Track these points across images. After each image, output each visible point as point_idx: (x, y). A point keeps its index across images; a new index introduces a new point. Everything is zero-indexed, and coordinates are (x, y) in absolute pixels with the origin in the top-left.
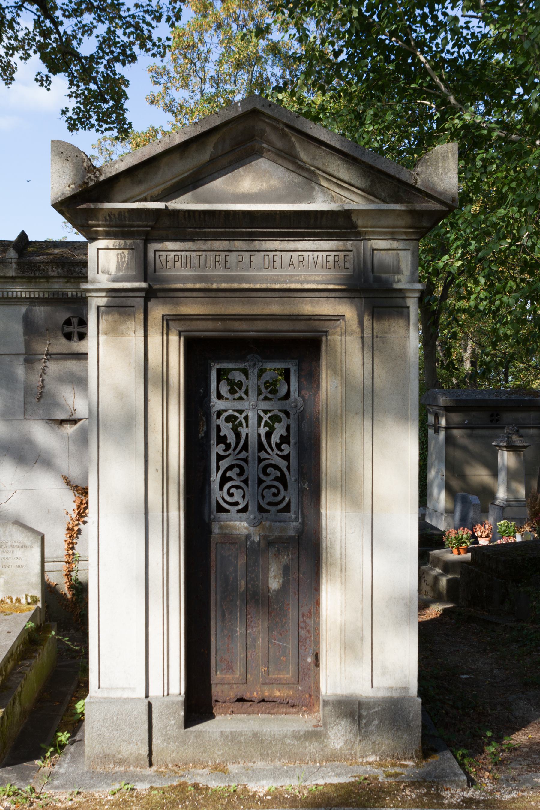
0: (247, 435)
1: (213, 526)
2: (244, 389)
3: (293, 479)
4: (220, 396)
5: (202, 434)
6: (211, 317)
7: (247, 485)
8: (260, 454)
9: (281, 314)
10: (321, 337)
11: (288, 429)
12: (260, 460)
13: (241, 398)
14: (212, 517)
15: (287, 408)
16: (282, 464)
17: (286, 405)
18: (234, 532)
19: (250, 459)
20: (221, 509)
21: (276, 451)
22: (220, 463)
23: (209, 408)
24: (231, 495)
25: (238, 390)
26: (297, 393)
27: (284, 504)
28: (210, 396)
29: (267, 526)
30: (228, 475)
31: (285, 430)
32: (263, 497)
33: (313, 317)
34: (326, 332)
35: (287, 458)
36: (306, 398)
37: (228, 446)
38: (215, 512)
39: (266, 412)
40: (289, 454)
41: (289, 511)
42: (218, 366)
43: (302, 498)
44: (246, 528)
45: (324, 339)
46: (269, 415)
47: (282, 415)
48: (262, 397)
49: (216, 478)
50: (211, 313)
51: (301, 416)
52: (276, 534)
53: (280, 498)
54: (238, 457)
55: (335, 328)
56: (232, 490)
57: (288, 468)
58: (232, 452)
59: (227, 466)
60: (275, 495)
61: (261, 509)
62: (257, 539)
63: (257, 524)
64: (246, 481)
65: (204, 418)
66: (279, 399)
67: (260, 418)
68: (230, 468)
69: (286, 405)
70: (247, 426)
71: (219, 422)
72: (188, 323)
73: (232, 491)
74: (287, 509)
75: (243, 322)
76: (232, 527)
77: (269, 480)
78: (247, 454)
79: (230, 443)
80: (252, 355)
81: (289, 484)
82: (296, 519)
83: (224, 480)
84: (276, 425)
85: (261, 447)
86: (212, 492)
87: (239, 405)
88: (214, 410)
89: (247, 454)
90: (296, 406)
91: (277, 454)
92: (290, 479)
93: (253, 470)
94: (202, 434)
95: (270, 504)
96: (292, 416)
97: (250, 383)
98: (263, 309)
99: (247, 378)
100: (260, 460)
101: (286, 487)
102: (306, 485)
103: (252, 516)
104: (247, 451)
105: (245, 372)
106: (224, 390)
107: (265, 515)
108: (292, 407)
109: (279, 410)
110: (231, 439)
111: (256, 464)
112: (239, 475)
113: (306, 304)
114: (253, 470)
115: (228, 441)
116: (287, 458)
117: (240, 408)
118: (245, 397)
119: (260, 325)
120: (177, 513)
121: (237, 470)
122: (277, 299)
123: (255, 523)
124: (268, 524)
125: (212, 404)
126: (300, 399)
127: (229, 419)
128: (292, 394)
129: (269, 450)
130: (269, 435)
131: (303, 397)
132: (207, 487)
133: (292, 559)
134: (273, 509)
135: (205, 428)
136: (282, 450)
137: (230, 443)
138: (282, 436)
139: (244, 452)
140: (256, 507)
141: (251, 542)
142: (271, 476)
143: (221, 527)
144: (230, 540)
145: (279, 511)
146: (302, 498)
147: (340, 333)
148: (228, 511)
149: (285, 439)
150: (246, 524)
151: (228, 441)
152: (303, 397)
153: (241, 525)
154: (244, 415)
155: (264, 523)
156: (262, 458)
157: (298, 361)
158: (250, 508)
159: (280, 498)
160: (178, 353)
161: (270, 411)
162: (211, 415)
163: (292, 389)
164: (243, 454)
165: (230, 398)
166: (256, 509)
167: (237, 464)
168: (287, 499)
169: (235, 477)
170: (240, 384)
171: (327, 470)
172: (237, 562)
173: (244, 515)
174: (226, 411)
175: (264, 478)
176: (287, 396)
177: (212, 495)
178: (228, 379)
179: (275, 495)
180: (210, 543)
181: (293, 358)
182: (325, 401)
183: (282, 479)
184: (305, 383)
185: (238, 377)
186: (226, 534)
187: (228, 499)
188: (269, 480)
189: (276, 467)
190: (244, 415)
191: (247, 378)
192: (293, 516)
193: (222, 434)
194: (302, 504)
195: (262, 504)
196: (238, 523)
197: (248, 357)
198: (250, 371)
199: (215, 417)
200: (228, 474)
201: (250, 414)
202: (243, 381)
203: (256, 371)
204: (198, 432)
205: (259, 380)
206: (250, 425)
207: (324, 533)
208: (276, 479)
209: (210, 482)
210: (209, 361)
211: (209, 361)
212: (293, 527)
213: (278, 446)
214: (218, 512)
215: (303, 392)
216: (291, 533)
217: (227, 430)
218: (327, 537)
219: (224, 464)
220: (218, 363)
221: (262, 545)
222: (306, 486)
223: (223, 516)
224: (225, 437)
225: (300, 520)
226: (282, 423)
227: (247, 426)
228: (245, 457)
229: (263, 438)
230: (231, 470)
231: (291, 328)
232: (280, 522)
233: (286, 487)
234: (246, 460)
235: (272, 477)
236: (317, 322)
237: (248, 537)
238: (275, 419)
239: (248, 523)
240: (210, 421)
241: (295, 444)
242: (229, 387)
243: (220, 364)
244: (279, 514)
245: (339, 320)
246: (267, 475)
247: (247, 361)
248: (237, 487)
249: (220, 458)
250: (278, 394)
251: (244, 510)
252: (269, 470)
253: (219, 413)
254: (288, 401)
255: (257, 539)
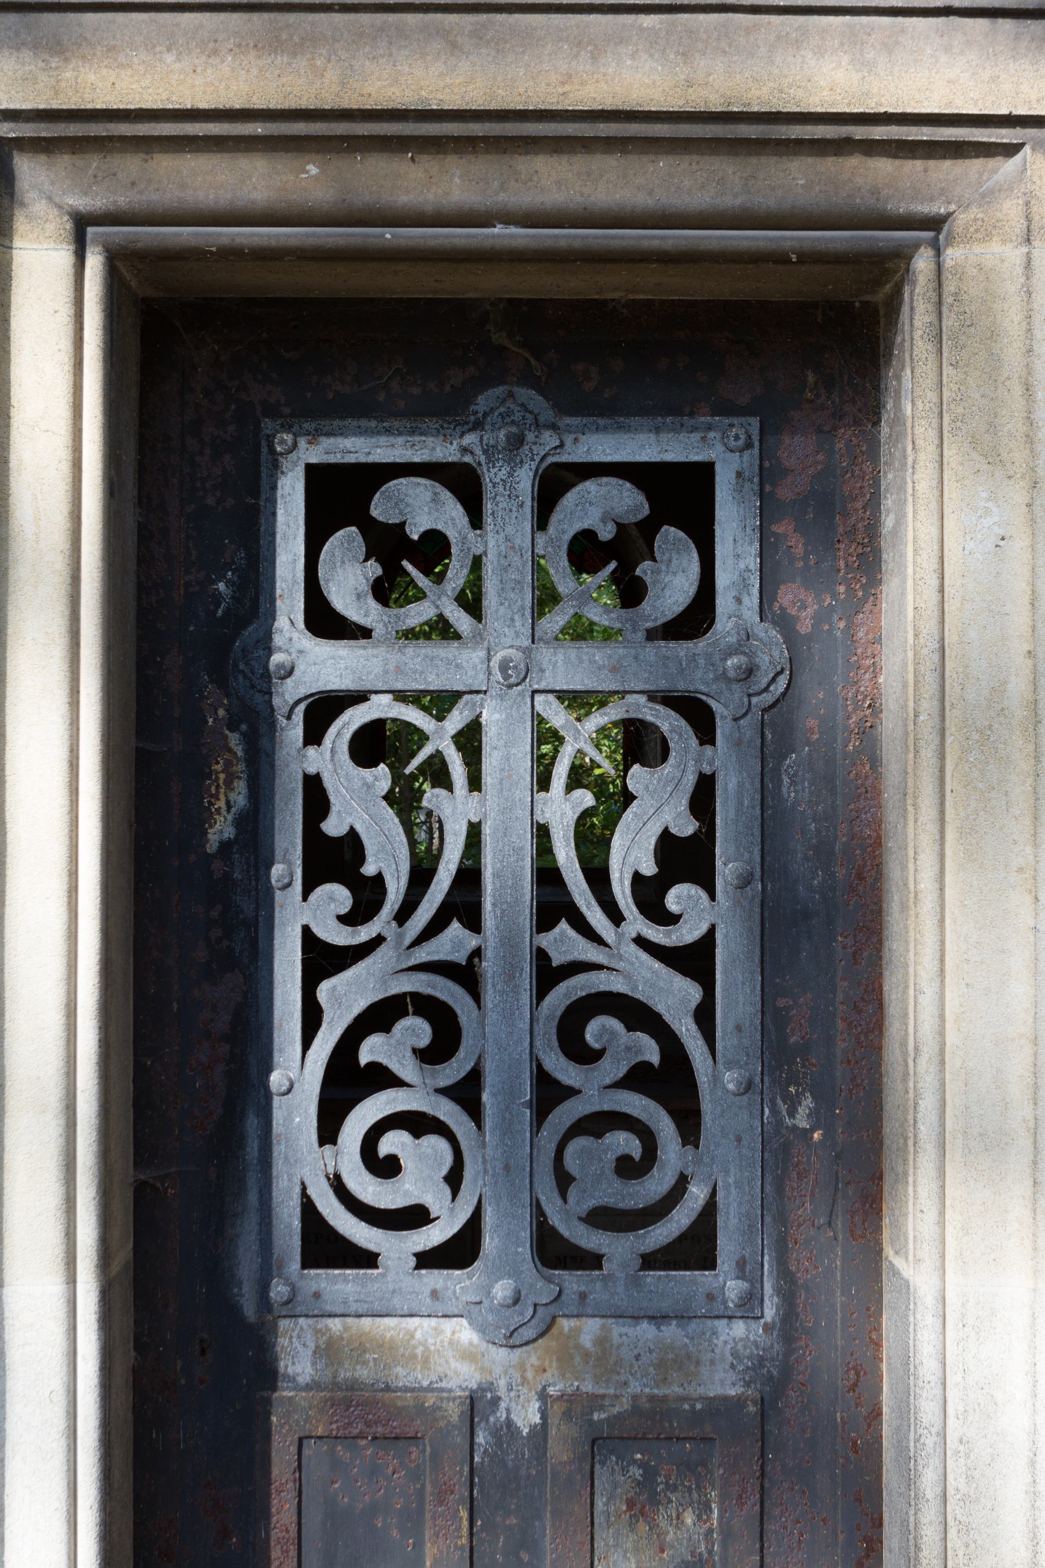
0: (474, 832)
1: (283, 1341)
2: (457, 575)
3: (730, 1079)
4: (324, 621)
5: (221, 829)
6: (258, 129)
7: (474, 1110)
8: (546, 940)
9: (675, 104)
10: (903, 256)
11: (703, 799)
12: (548, 974)
13: (441, 629)
14: (278, 1290)
15: (697, 682)
16: (673, 995)
17: (691, 664)
18: (403, 1375)
19: (488, 966)
20: (326, 1248)
21: (636, 923)
22: (324, 991)
23: (264, 681)
24: (386, 1168)
25: (422, 581)
26: (752, 600)
27: (681, 1219)
28: (272, 615)
29: (587, 1340)
30: (365, 1057)
31: (683, 804)
32: (564, 1180)
33: (859, 132)
34: (935, 224)
35: (695, 960)
36: (805, 627)
37: (367, 898)
38: (295, 1265)
39: (578, 701)
40: (708, 940)
41: (709, 1263)
42: (316, 453)
43: (780, 1190)
44: (468, 1355)
45: (922, 263)
46: (597, 720)
47: (668, 722)
48: (556, 621)
49: (297, 1074)
50: (258, 102)
51: (775, 735)
52: (635, 1387)
53: (655, 1185)
54: (423, 954)
55: (988, 197)
56: (391, 1143)
57: (705, 1016)
58: (390, 930)
59: (360, 1005)
60: (629, 1169)
61: (553, 1251)
62: (527, 1415)
63: (528, 1333)
64: (467, 1093)
65: (234, 740)
66: (652, 635)
67: (546, 736)
68: (379, 1017)
69: (691, 664)
70: (475, 783)
71: (315, 760)
72: (130, 164)
73: (391, 1143)
74: (696, 1249)
75: (451, 160)
76: (388, 1349)
77: (593, 1089)
78: (473, 941)
79: (379, 879)
80: (500, 390)
81: (706, 1106)
82: (749, 1306)
83: (348, 1080)
84: (638, 777)
85: (552, 905)
86: (279, 1150)
87: (432, 667)
88: (290, 692)
89: (473, 941)
90: (750, 672)
91: (641, 942)
92: (716, 1079)
93: (505, 1030)
94: (221, 829)
95: (604, 1218)
96: (722, 729)
97: (492, 543)
98: (568, 78)
99: (476, 520)
100: (548, 974)
101: (689, 1124)
102: (802, 1111)
103: (502, 1290)
104: (474, 924)
105: (465, 485)
106: (348, 583)
107: (573, 1280)
108: (724, 676)
109: (653, 697)
110: (387, 857)
111: (525, 998)
112: (432, 1055)
113: (820, 52)
114: (505, 1030)
115: (369, 869)
116: (695, 960)
117: (435, 681)
118: (461, 620)
119: (553, 181)
120: (55, 1287)
121: (414, 1029)
122: (648, 21)
123: (523, 1328)
124: (589, 1329)
125: (277, 658)
126: (768, 632)
127: (373, 745)
128: (723, 603)
129: (596, 917)
130: (593, 840)
131: (785, 624)
132: (252, 1123)
133: (727, 1534)
134: (619, 1249)
135: (240, 797)
136: (670, 919)
137: (379, 879)
138: (667, 842)
139: (455, 927)
140: (525, 1235)
141: (496, 1433)
142: (605, 1063)
143: (329, 1351)
144: (376, 1417)
145: (650, 1261)
146: (780, 1190)
147: (1018, 225)
148: (367, 1259)
149: (684, 859)
150: (465, 1333)
151: (369, 869)
152: (785, 624)
153: (439, 1337)
154: (456, 720)
155: (566, 1324)
156: (558, 959)
157: (755, 422)
158: (489, 1243)
159: (655, 1185)
160: (65, 344)
161: (601, 699)
162: (272, 725)
163: (723, 579)
164: (454, 942)
165: (378, 631)
166: (525, 1250)
167: (415, 996)
168: (697, 1194)
169: (406, 1068)
170: (433, 550)
171: (942, 1033)
172: (419, 1545)
173: (454, 1282)
174: (360, 697)
175: (566, 1072)
176: (697, 617)
177: (279, 1166)
178: (371, 529)
179: (629, 1169)
180: (887, 125)
181: (726, 409)
182: (929, 626)
183: (670, 1080)
184: (797, 544)
185: (422, 508)
186: (353, 1386)
187: (369, 1189)
188: (593, 1089)
189: (637, 1014)
190: (456, 720)
191: (476, 520)
192: (734, 1288)
193: (333, 827)
194: (782, 1218)
195: (555, 1220)
196: (421, 1328)
197: (482, 403)
198: (492, 476)
199: (295, 731)
200: (372, 1050)
201: (491, 716)
202: (452, 534)
203: (525, 480)
204: (203, 818)
205: (542, 522)
206: (488, 778)
207: (927, 1409)
208: (638, 1078)
209: (268, 1096)
210: (268, 425)
211: (268, 425)
212: (728, 1348)
213: (650, 895)
214: (310, 1261)
215: (786, 597)
216: (722, 1383)
217: (359, 804)
218: (943, 1435)
219: (346, 996)
220: (314, 436)
221: (558, 1451)
222: (802, 1121)
223: (339, 1284)
224: (353, 840)
225: (770, 1313)
226: (668, 769)
227: (475, 783)
228: (460, 957)
229: (565, 855)
230: (386, 1027)
231: (731, 200)
232: (659, 1319)
233: (689, 1124)
234: (466, 974)
235: (611, 1068)
236: (884, 166)
237: (477, 1404)
238: (638, 744)
239: (482, 1329)
240: (270, 756)
241: (744, 882)
242: (374, 569)
243: (326, 442)
244: (652, 1276)
245: (1011, 150)
246: (583, 1054)
247: (478, 426)
248: (417, 1124)
249: (322, 960)
250: (646, 606)
251: (460, 1252)
252: (594, 1031)
253: (323, 709)
254: (701, 645)
255: (527, 1415)
